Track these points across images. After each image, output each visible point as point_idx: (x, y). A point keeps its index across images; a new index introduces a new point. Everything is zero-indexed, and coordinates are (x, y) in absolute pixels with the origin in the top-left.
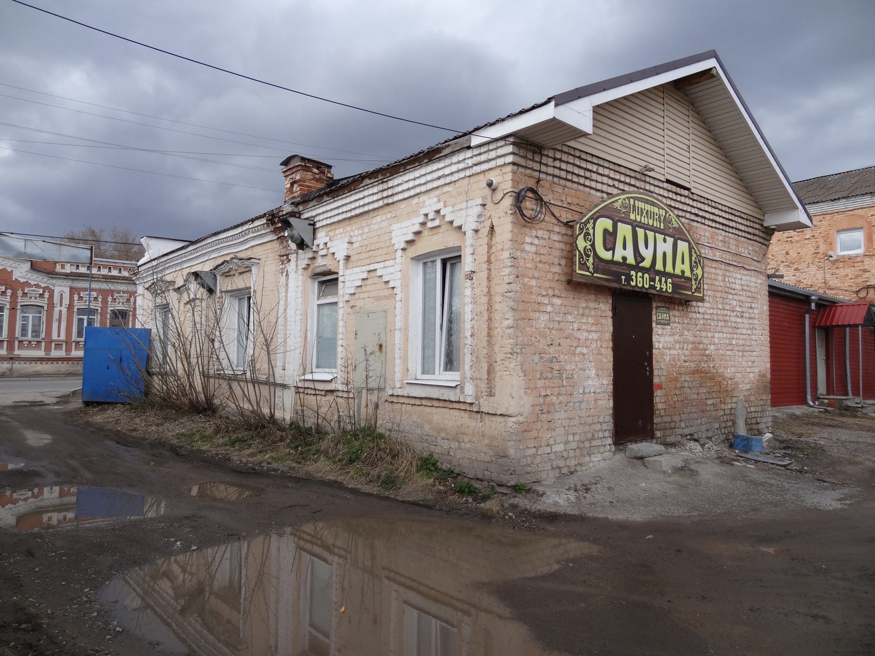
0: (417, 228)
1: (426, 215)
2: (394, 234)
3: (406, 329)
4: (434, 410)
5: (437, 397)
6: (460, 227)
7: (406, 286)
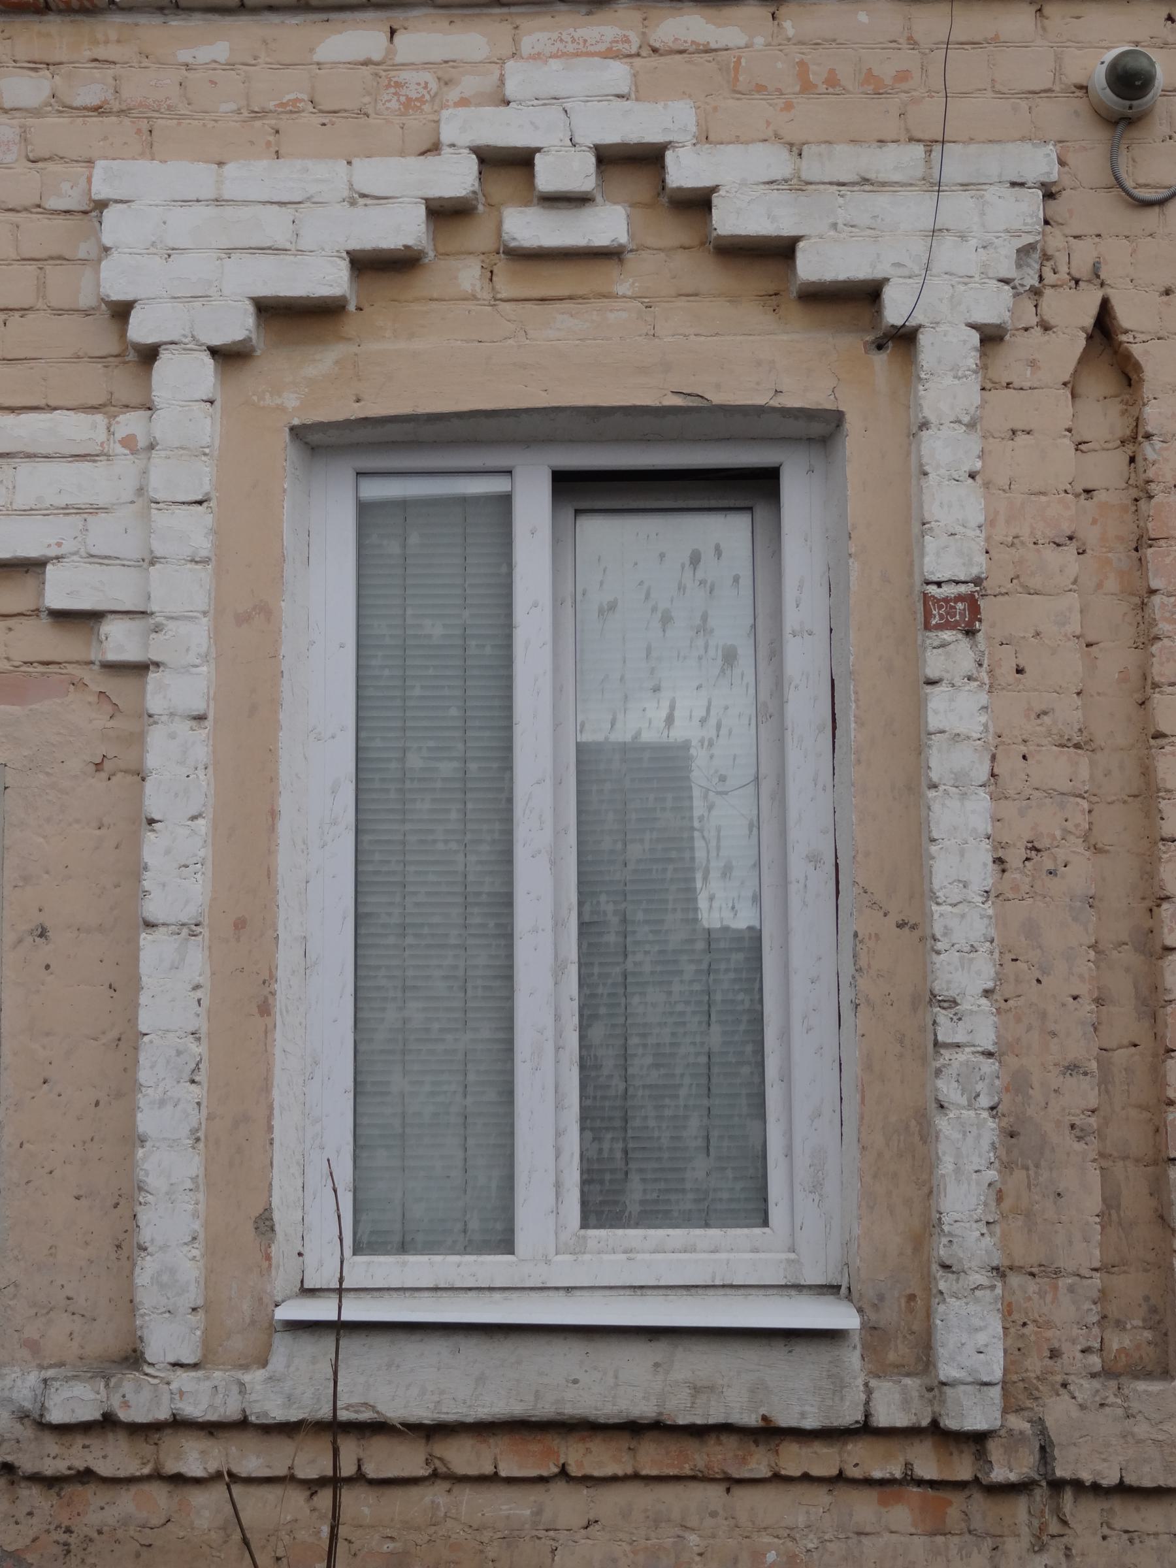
0: (404, 228)
1: (509, 164)
2: (115, 226)
3: (243, 927)
4: (566, 1505)
5: (643, 1409)
6: (149, 355)
7: (250, 618)
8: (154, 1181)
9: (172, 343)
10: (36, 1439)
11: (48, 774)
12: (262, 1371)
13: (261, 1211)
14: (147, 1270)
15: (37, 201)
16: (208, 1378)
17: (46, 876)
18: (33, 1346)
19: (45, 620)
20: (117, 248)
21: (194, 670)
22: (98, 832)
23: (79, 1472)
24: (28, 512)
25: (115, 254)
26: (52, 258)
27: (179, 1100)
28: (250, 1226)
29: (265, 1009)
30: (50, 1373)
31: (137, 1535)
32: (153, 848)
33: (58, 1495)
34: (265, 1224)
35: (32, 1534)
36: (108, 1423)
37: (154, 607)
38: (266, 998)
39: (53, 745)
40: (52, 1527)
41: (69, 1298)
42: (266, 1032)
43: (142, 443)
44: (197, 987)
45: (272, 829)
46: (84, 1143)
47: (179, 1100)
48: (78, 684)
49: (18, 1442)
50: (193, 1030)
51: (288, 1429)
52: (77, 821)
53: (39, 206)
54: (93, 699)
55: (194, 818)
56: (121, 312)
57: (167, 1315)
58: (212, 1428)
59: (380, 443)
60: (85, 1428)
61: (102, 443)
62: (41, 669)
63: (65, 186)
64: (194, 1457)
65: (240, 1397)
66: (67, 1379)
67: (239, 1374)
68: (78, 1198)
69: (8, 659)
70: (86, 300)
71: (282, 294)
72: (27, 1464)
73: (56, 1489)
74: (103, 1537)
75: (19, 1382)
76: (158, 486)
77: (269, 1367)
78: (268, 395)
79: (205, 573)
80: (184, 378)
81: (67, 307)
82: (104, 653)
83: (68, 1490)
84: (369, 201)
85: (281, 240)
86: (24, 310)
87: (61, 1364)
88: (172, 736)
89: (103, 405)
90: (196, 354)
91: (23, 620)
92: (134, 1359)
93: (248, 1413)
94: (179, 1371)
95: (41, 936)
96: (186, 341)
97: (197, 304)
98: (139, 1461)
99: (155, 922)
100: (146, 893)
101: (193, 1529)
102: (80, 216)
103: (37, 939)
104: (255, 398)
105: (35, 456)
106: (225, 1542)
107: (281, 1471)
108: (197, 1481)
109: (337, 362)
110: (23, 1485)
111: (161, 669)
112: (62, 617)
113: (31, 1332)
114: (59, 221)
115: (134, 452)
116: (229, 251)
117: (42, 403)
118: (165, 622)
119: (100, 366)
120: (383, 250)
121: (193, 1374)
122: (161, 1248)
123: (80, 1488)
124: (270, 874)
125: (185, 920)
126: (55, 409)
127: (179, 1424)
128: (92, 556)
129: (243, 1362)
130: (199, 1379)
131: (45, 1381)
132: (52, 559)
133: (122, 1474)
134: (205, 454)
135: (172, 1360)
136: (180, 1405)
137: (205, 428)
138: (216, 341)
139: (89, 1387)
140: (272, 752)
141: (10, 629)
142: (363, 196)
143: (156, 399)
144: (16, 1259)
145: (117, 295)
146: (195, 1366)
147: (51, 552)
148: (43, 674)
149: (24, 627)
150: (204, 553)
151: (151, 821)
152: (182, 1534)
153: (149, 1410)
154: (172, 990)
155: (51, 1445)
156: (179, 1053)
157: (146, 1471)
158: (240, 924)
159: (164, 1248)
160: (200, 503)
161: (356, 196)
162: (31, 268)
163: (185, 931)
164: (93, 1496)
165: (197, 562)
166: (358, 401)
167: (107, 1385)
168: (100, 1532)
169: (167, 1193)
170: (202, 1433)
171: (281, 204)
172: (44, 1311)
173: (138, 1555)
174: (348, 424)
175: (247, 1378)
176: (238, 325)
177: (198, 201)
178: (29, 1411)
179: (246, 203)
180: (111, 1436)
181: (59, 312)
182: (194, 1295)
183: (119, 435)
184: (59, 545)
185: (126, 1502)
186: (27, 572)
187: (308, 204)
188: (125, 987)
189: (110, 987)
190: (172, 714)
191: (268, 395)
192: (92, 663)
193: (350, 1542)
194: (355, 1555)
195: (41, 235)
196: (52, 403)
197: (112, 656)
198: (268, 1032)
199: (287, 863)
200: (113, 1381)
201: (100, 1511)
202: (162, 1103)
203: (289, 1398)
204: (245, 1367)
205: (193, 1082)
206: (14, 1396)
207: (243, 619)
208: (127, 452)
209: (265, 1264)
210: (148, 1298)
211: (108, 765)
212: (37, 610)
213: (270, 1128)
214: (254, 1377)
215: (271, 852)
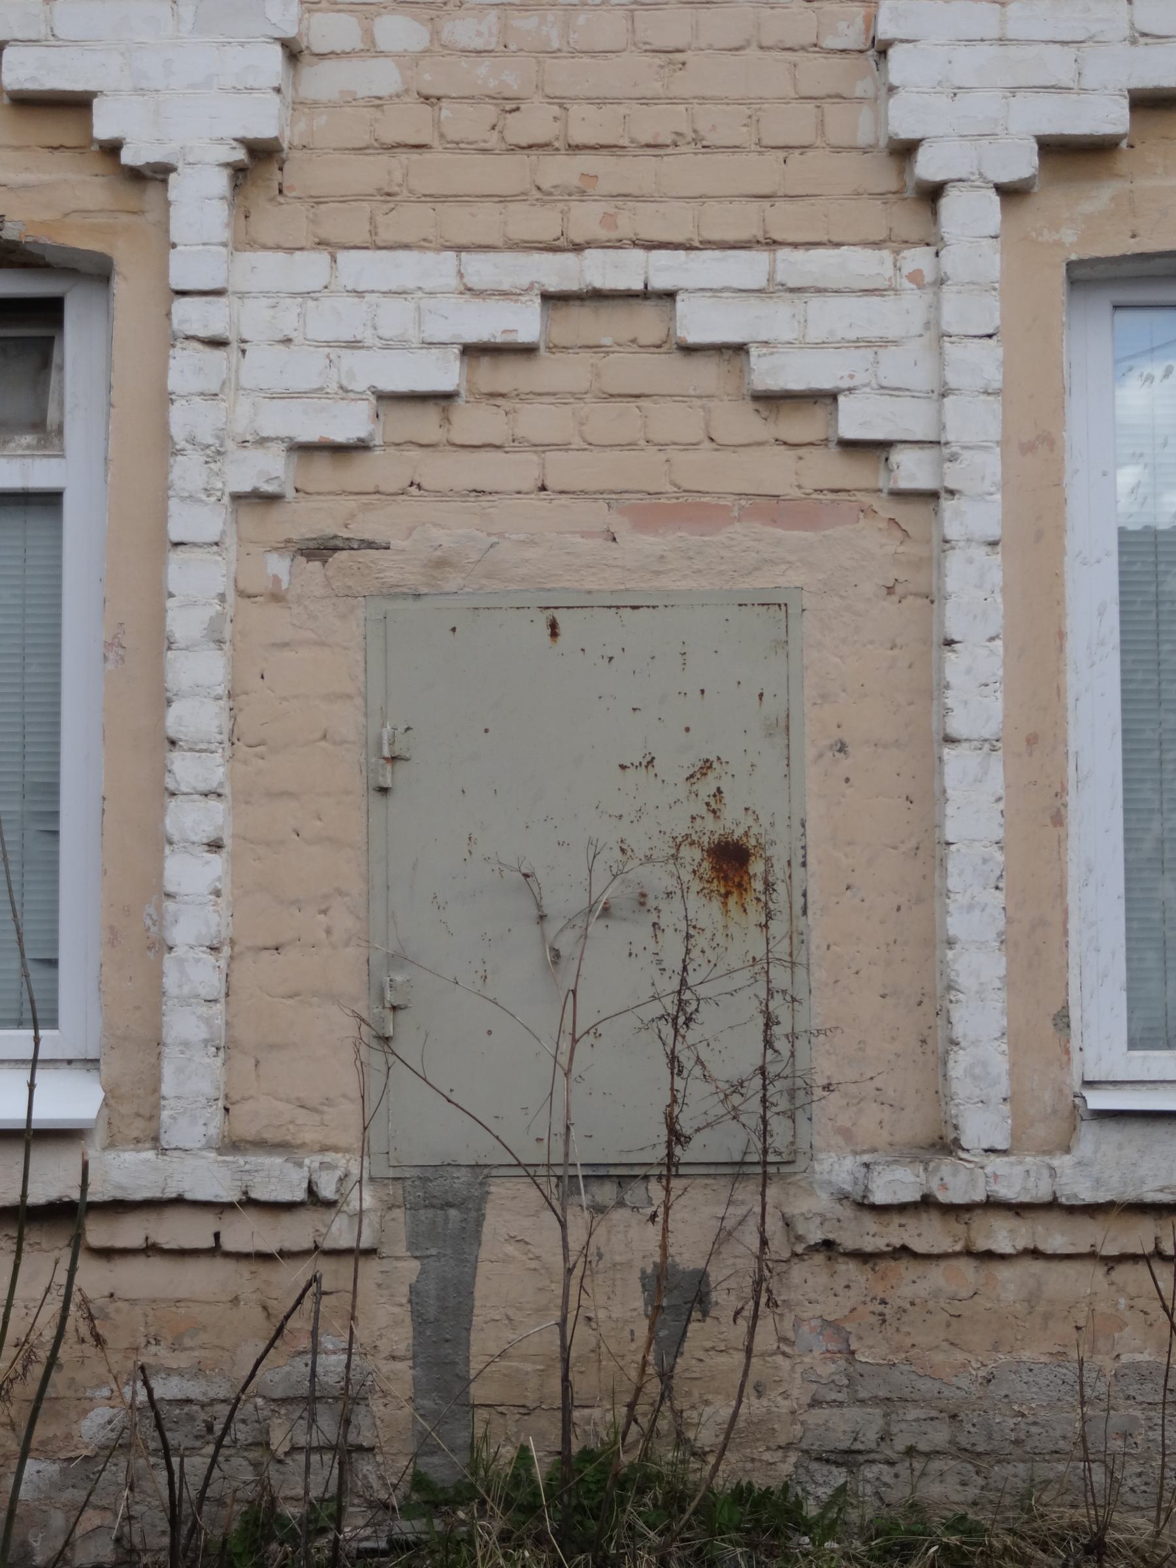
3: (1035, 742)
6: (932, 194)
8: (964, 980)
9: (960, 180)
10: (856, 1218)
11: (841, 597)
12: (1067, 1158)
13: (1059, 1008)
14: (960, 1064)
15: (814, 41)
16: (1021, 1163)
17: (843, 694)
18: (847, 1134)
19: (834, 449)
20: (905, 87)
21: (988, 498)
22: (890, 653)
23: (895, 1248)
24: (820, 345)
25: (902, 93)
26: (830, 97)
27: (986, 905)
28: (1049, 1023)
29: (1058, 820)
30: (866, 1158)
31: (946, 1307)
32: (955, 666)
33: (873, 1270)
34: (1062, 1020)
35: (850, 1305)
36: (927, 1203)
37: (950, 436)
38: (1059, 810)
39: (847, 569)
40: (868, 1299)
41: (878, 1089)
42: (1059, 842)
43: (929, 277)
44: (999, 799)
45: (1061, 649)
46: (888, 945)
47: (986, 905)
48: (868, 512)
49: (839, 1221)
50: (997, 839)
51: (1092, 1210)
52: (871, 642)
53: (815, 45)
54: (883, 525)
55: (992, 639)
56: (905, 151)
57: (980, 1105)
58: (1019, 1209)
59: (1137, 277)
60: (902, 1208)
61: (890, 279)
62: (831, 496)
63: (842, 26)
64: (1003, 1235)
65: (1050, 1180)
66: (888, 1164)
67: (1047, 1159)
68: (883, 997)
69: (799, 487)
70: (864, 136)
71: (1066, 132)
72: (848, 1241)
73: (870, 1265)
74: (916, 1308)
75: (836, 1166)
76: (950, 320)
77: (1074, 1152)
78: (1045, 232)
79: (996, 404)
80: (970, 215)
81: (846, 145)
82: (895, 482)
83: (882, 1265)
84: (1149, 40)
85: (1066, 81)
86: (804, 148)
87: (874, 1150)
88: (970, 561)
89: (883, 241)
90: (984, 191)
91: (812, 449)
92: (946, 1145)
93: (1058, 1195)
94: (993, 1157)
95: (840, 751)
96: (973, 178)
97: (985, 142)
98: (951, 1239)
99: (958, 737)
100: (948, 710)
101: (999, 1300)
102: (856, 55)
103: (837, 754)
104: (1034, 234)
105: (825, 290)
106: (1030, 1313)
107: (1084, 1248)
108: (1003, 1257)
109: (1112, 199)
110: (841, 1260)
111: (957, 496)
112: (849, 445)
113: (844, 1120)
114: (836, 60)
115: (921, 286)
116: (1014, 90)
117: (825, 239)
118: (960, 452)
119: (879, 202)
120: (1164, 89)
121: (1006, 1159)
122: (973, 1043)
123: (893, 1263)
124: (1059, 692)
125: (988, 736)
126: (842, 244)
127: (992, 1205)
128: (882, 388)
129: (1045, 1148)
130: (1012, 1164)
131: (867, 1165)
132: (844, 390)
133: (935, 1251)
134: (995, 289)
135: (986, 1147)
136: (994, 1187)
137: (992, 263)
138: (1004, 178)
139: (909, 1171)
140: (1058, 576)
141: (800, 458)
142: (1144, 35)
143: (945, 235)
144: (828, 1052)
145: (905, 131)
146: (1004, 1152)
147: (844, 384)
148: (833, 501)
149: (814, 456)
150: (996, 385)
151: (949, 643)
152: (989, 1305)
153: (966, 1192)
154: (974, 802)
155: (870, 1223)
156: (985, 861)
157: (958, 1247)
158: (1032, 740)
159: (976, 1043)
160: (990, 336)
161: (1137, 35)
162: (810, 106)
163: (987, 746)
164: (906, 1270)
165: (989, 394)
166: (1134, 236)
167: (926, 1169)
168: (912, 1304)
169: (977, 992)
170: (1010, 1214)
171: (1064, 43)
172: (855, 1101)
173: (948, 1325)
174: (1124, 258)
175: (1056, 1162)
176: (1023, 163)
177: (982, 40)
178: (849, 1193)
179: (1030, 42)
180: (924, 1216)
181: (838, 149)
182: (1004, 1088)
183: (906, 270)
184: (852, 377)
185: (937, 1276)
186: (815, 403)
187: (1091, 43)
188: (926, 798)
189: (907, 798)
190: (969, 540)
191: (1045, 232)
192: (880, 491)
193: (1146, 1313)
194: (1151, 1325)
195: (819, 74)
196: (835, 239)
197: (904, 485)
198: (1061, 841)
199: (1074, 682)
200: (932, 1165)
201: (911, 1284)
202: (970, 908)
203: (1097, 1181)
204: (1049, 1153)
205: (997, 888)
206: (834, 1178)
207: (1028, 448)
208: (914, 286)
209: (1065, 1058)
210: (962, 1087)
211: (899, 589)
212: (827, 439)
213: (1066, 932)
214: (1062, 1162)
215: (1060, 671)
